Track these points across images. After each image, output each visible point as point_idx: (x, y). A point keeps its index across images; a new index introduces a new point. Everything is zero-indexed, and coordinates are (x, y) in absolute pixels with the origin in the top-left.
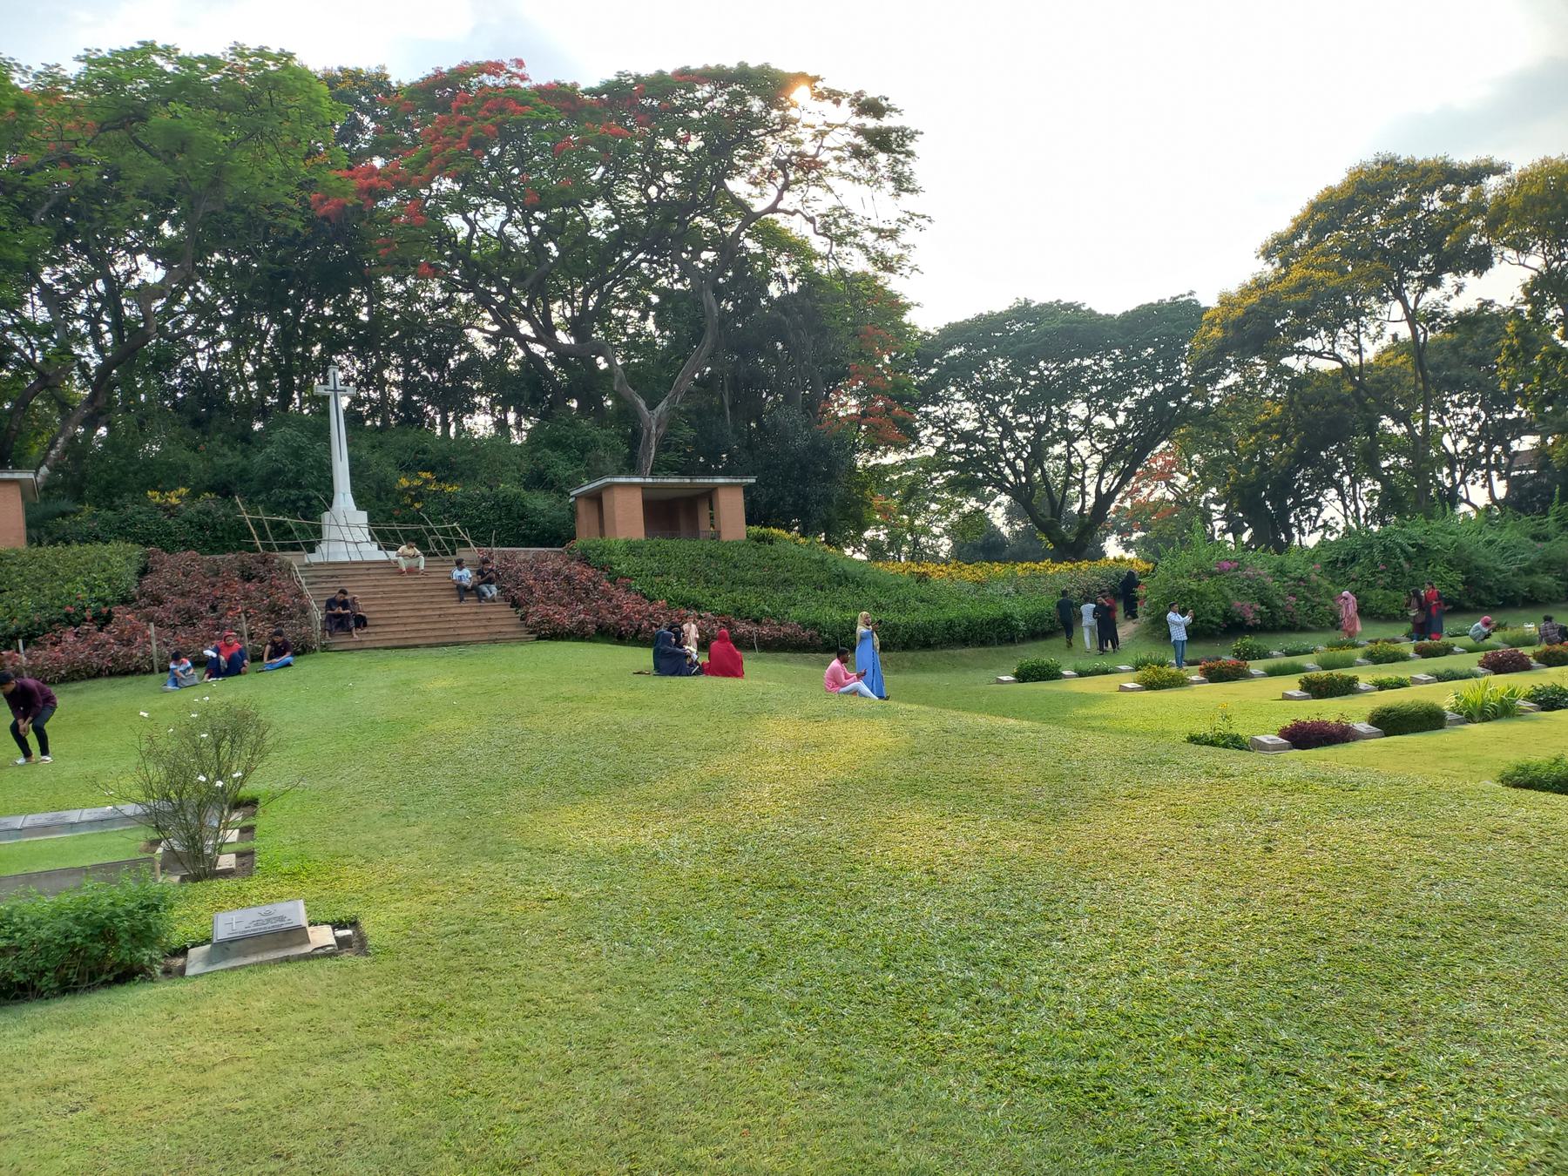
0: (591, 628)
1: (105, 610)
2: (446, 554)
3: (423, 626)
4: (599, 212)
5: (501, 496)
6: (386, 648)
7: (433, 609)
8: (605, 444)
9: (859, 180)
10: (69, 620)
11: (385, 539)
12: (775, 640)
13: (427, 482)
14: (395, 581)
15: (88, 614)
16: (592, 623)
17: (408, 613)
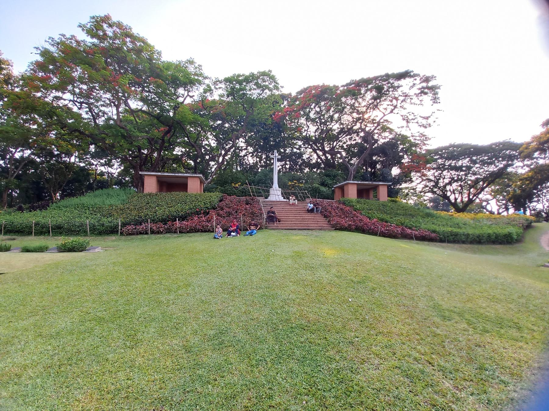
1: (208, 211)
3: (297, 222)
6: (285, 229)
7: (300, 217)
10: (197, 213)
11: (286, 195)
13: (295, 183)
16: (354, 225)
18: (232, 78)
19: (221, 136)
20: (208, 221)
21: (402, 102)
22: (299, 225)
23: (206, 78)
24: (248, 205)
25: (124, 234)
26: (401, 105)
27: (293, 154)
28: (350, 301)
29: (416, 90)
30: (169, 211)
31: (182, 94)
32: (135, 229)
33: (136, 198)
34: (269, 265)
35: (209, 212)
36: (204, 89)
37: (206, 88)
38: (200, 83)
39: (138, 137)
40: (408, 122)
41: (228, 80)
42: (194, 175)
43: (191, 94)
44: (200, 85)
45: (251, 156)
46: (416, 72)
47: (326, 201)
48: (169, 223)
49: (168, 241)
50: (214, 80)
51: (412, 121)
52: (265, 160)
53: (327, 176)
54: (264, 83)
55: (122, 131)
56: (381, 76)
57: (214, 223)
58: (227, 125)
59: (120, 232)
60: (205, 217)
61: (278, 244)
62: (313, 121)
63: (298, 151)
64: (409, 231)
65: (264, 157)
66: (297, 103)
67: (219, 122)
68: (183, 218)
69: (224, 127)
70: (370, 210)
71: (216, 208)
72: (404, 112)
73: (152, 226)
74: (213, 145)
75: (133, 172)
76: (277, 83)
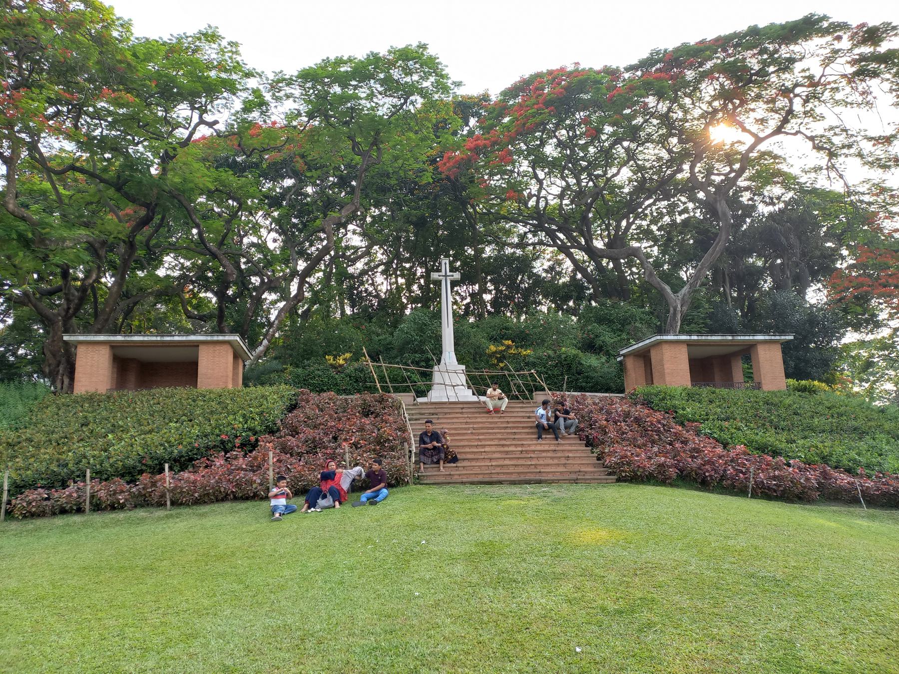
0: (673, 472)
1: (253, 438)
2: (527, 399)
3: (507, 462)
4: (626, 174)
5: (563, 356)
6: (472, 483)
7: (516, 445)
8: (641, 319)
9: (851, 104)
10: (225, 447)
11: (477, 384)
12: (885, 494)
13: (509, 347)
14: (482, 419)
15: (238, 442)
17: (494, 449)
18: (320, 72)
19: (294, 220)
20: (255, 468)
21: (806, 101)
22: (511, 470)
23: (248, 75)
24: (367, 416)
25: (17, 513)
26: (808, 109)
27: (502, 261)
28: (577, 653)
29: (842, 67)
30: (145, 445)
31: (186, 119)
32: (48, 499)
33: (53, 409)
34: (405, 579)
35: (257, 440)
36: (244, 102)
37: (250, 98)
38: (232, 88)
39: (64, 240)
40: (832, 155)
41: (307, 76)
42: (215, 338)
43: (208, 118)
44: (234, 94)
45: (383, 273)
46: (836, 18)
47: (593, 398)
48: (145, 478)
49: (140, 529)
50: (271, 77)
51: (845, 151)
52: (422, 281)
53: (602, 320)
54: (408, 79)
55: (22, 226)
56: (735, 35)
57: (271, 473)
58: (309, 190)
59: (6, 511)
60: (245, 456)
61: (442, 524)
62: (554, 166)
63: (519, 252)
64: (844, 479)
65: (420, 271)
66: (506, 120)
67: (288, 182)
68: (182, 463)
69: (301, 194)
70: (727, 419)
71: (278, 430)
72: (817, 128)
73: (96, 489)
74: (271, 245)
75: (41, 331)
76: (442, 76)
